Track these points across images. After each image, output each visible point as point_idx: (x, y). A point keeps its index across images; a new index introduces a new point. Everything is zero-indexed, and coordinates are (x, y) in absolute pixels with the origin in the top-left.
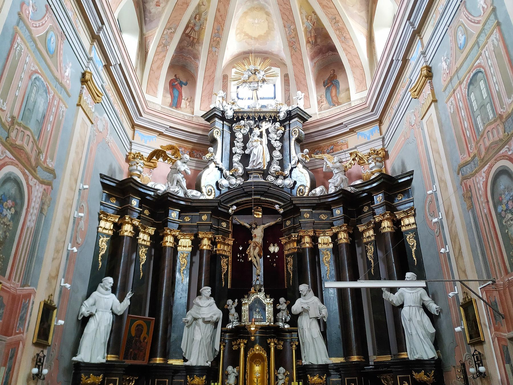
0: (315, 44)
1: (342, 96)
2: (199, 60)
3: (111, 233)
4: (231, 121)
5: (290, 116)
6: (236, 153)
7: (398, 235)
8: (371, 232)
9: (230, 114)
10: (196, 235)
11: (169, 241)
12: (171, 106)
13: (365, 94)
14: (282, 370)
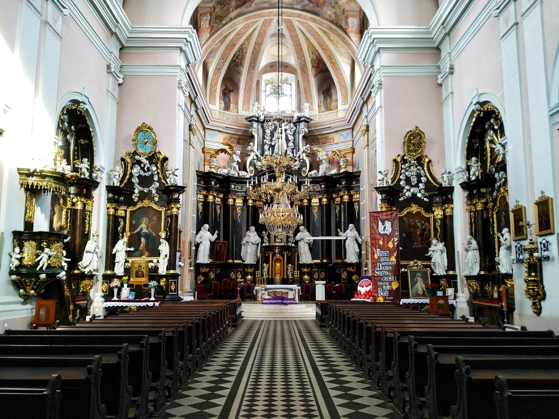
0: (317, 67)
1: (333, 104)
2: (241, 76)
3: (203, 200)
4: (263, 122)
5: (299, 120)
6: (266, 144)
7: (351, 203)
8: (338, 199)
9: (262, 118)
10: (245, 197)
11: (231, 201)
12: (224, 110)
13: (346, 107)
14: (290, 265)
